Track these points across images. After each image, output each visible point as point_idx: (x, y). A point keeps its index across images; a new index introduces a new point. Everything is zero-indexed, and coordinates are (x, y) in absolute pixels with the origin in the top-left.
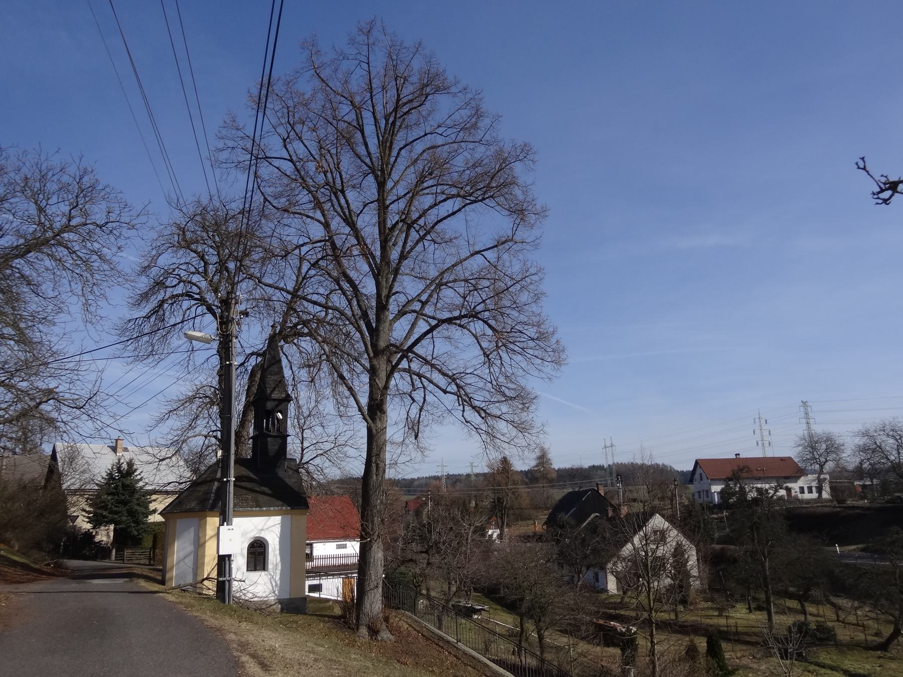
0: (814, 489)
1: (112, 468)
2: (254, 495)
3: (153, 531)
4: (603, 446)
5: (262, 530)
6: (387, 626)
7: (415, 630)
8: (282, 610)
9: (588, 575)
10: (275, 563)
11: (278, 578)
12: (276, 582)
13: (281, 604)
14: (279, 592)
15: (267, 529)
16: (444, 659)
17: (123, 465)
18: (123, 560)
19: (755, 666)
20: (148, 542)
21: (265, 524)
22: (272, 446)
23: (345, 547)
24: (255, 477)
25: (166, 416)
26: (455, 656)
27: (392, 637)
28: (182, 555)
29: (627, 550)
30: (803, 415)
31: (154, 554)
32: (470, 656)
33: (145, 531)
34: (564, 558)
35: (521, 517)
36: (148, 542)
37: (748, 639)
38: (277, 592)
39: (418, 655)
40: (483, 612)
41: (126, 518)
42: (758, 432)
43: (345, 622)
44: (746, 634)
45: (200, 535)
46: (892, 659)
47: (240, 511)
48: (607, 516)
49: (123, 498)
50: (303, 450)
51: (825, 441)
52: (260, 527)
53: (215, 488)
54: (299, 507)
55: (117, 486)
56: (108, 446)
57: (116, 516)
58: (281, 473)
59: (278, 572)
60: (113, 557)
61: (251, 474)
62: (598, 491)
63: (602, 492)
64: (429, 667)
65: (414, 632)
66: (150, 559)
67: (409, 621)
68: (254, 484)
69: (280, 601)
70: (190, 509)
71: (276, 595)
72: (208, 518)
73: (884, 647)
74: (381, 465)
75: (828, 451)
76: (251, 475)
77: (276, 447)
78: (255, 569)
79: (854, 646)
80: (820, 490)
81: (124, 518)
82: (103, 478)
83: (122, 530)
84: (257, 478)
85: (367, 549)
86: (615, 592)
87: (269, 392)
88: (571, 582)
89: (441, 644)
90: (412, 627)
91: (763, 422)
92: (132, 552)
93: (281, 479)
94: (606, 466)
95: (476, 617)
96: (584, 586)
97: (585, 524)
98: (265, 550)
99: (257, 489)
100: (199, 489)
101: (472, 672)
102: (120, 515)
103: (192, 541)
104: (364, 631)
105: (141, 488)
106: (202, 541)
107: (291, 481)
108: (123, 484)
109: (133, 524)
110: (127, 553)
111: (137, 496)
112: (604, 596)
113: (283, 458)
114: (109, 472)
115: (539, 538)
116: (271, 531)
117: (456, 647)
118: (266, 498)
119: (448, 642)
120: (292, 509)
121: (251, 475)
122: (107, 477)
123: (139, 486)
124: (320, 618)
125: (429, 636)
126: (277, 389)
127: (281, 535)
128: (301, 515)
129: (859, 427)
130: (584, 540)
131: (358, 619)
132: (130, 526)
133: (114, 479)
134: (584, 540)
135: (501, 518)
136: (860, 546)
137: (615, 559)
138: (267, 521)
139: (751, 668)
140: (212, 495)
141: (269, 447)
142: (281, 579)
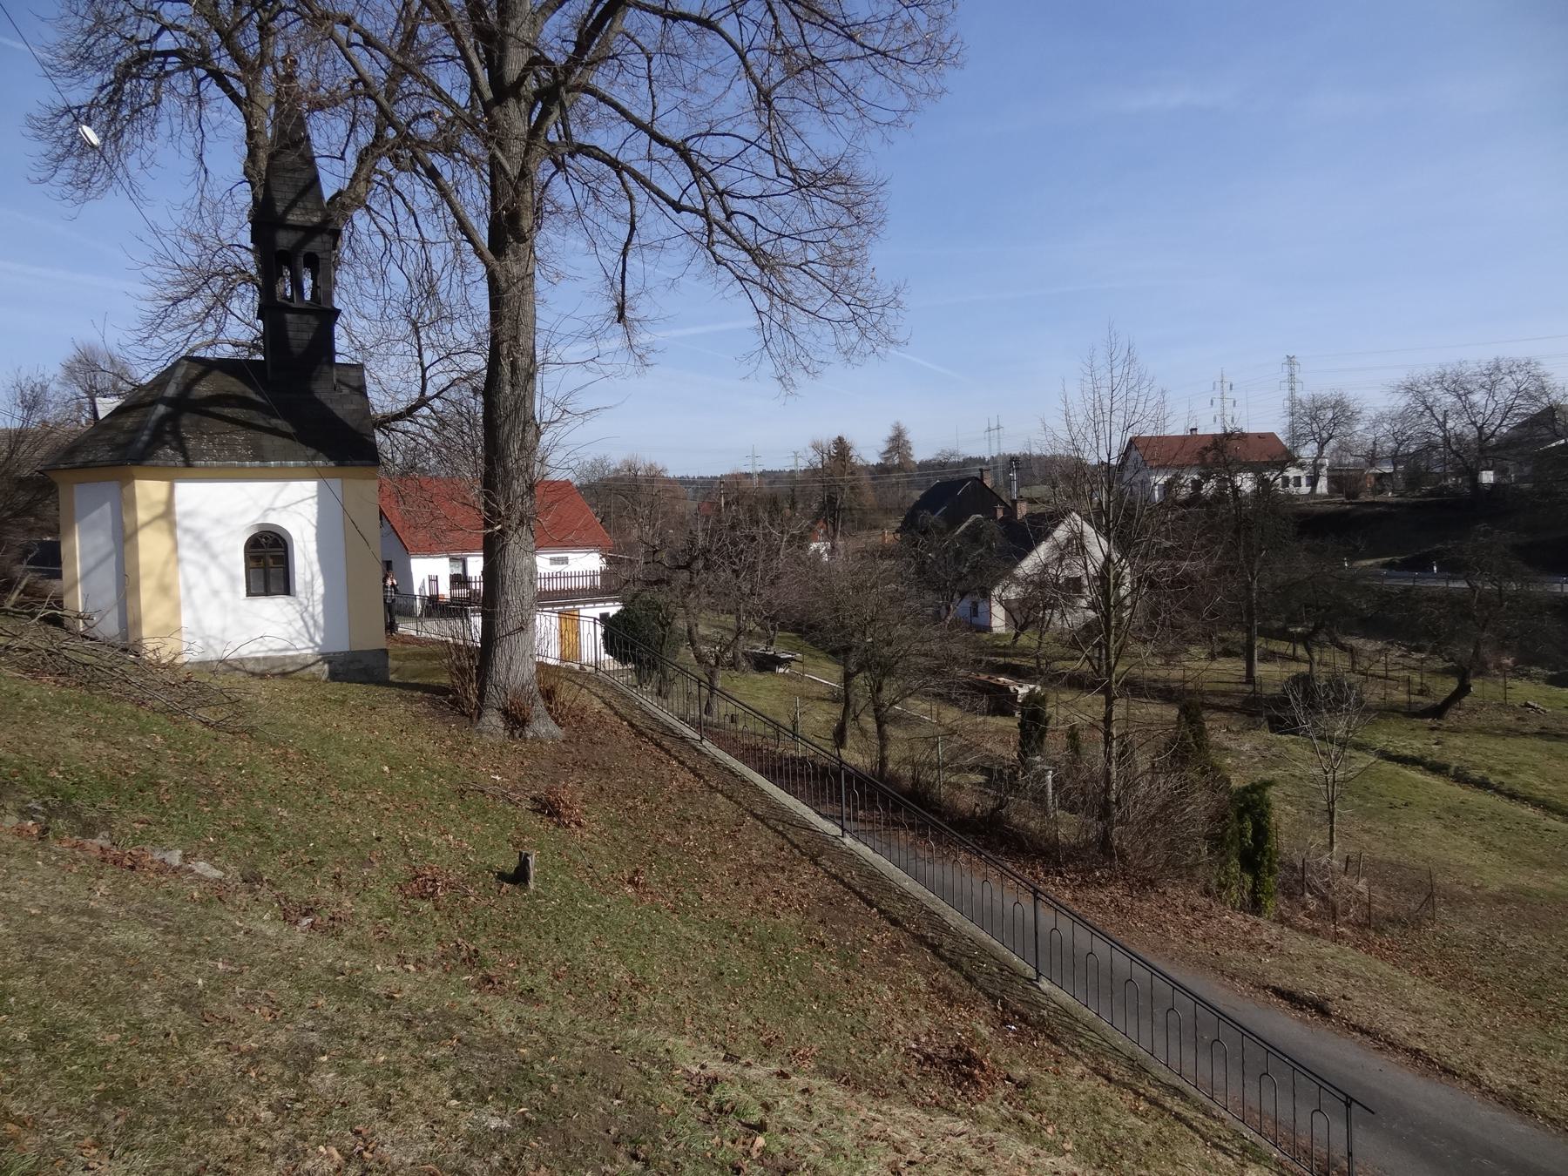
0: (1304, 481)
2: (251, 434)
6: (548, 709)
7: (616, 713)
9: (961, 607)
10: (308, 578)
12: (315, 622)
13: (330, 662)
14: (322, 640)
16: (667, 776)
19: (1233, 745)
21: (276, 497)
22: (299, 332)
23: (565, 561)
26: (693, 770)
27: (559, 733)
28: (91, 561)
29: (1028, 566)
30: (1285, 376)
32: (725, 769)
34: (925, 577)
35: (865, 523)
37: (1217, 701)
38: (318, 640)
39: (607, 771)
40: (793, 663)
42: (1217, 402)
43: (455, 703)
44: (1214, 693)
46: (1455, 731)
47: (212, 467)
48: (995, 517)
50: (424, 371)
51: (1334, 408)
52: (265, 503)
58: (322, 392)
62: (981, 481)
63: (988, 482)
64: (627, 797)
65: (616, 718)
67: (607, 695)
68: (254, 413)
69: (327, 658)
71: (317, 645)
73: (1438, 711)
74: (523, 362)
75: (1335, 421)
76: (252, 395)
77: (307, 336)
78: (267, 592)
79: (1389, 711)
80: (1313, 482)
85: (497, 549)
86: (1002, 630)
88: (937, 617)
89: (666, 743)
90: (612, 708)
91: (1226, 386)
93: (322, 405)
94: (988, 457)
95: (781, 670)
96: (955, 624)
97: (963, 527)
99: (261, 423)
101: (722, 808)
104: (493, 720)
106: (129, 530)
107: (343, 409)
112: (986, 636)
115: (885, 553)
117: (697, 750)
118: (279, 441)
119: (683, 739)
120: (337, 465)
121: (252, 395)
124: (405, 693)
125: (642, 727)
127: (319, 521)
129: (1402, 376)
130: (958, 553)
131: (481, 696)
134: (958, 553)
135: (833, 525)
136: (1380, 560)
137: (1006, 582)
138: (281, 491)
139: (1227, 749)
141: (291, 334)
142: (326, 611)
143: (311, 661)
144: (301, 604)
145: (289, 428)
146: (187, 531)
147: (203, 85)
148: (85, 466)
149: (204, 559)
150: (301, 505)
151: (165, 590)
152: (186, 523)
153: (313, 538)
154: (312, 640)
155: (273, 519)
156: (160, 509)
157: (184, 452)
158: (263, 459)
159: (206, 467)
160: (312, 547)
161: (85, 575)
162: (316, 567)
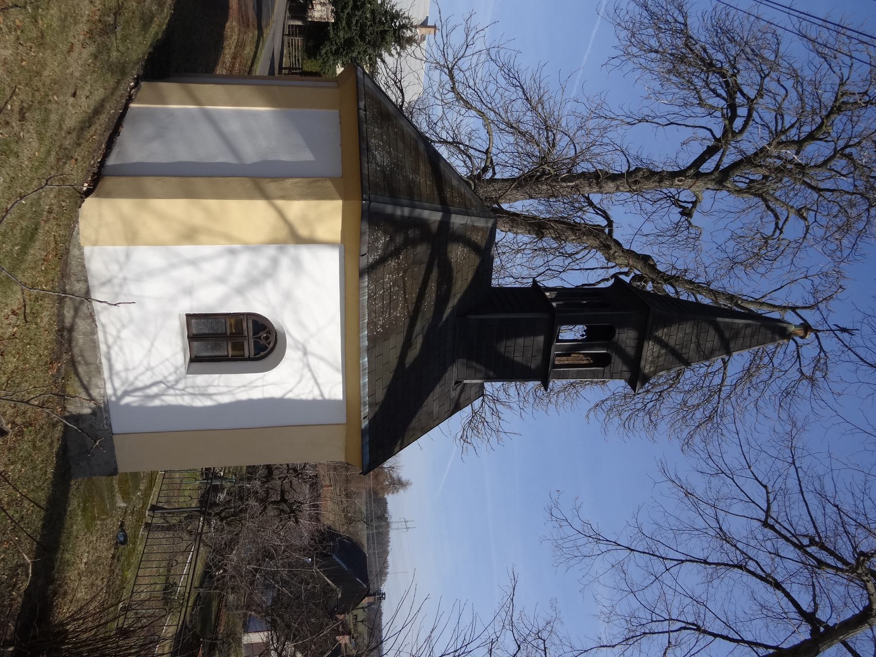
1: (405, 18)
2: (404, 322)
3: (324, 73)
4: (407, 519)
5: (305, 353)
8: (77, 419)
10: (211, 390)
11: (170, 399)
12: (156, 396)
13: (94, 413)
14: (127, 405)
15: (308, 366)
17: (409, 32)
18: (289, 35)
20: (310, 66)
21: (321, 358)
24: (448, 311)
25: (514, 81)
28: (233, 127)
31: (296, 74)
33: (325, 63)
36: (310, 66)
38: (127, 400)
41: (342, 36)
45: (289, 182)
47: (359, 295)
49: (368, 32)
52: (312, 346)
53: (426, 214)
54: (367, 449)
55: (384, 24)
56: (427, 17)
57: (344, 23)
59: (186, 401)
60: (292, 23)
61: (456, 301)
66: (290, 69)
69: (101, 412)
70: (368, 149)
71: (120, 398)
72: (338, 204)
76: (453, 302)
77: (518, 358)
81: (341, 34)
82: (393, 6)
83: (327, 33)
84: (440, 325)
87: (659, 333)
92: (298, 47)
98: (250, 359)
100: (422, 167)
102: (346, 29)
103: (272, 158)
105: (380, 56)
106: (271, 187)
108: (384, 32)
109: (334, 48)
110: (299, 40)
111: (370, 51)
112: (239, 629)
113: (491, 374)
114: (401, 13)
116: (302, 377)
121: (453, 302)
122: (394, 11)
123: (383, 52)
126: (663, 351)
127: (291, 401)
128: (346, 448)
132: (332, 44)
133: (392, 21)
138: (330, 364)
140: (406, 211)
141: (520, 341)
143: (95, 393)
144: (177, 381)
145: (410, 359)
146: (275, 262)
147: (658, 44)
148: (362, 139)
149: (236, 280)
150: (312, 382)
151: (190, 235)
152: (285, 262)
153: (267, 395)
154: (126, 393)
155: (291, 354)
156: (303, 232)
157: (382, 261)
158: (369, 349)
159: (359, 288)
160: (256, 394)
161: (209, 117)
162: (226, 399)
